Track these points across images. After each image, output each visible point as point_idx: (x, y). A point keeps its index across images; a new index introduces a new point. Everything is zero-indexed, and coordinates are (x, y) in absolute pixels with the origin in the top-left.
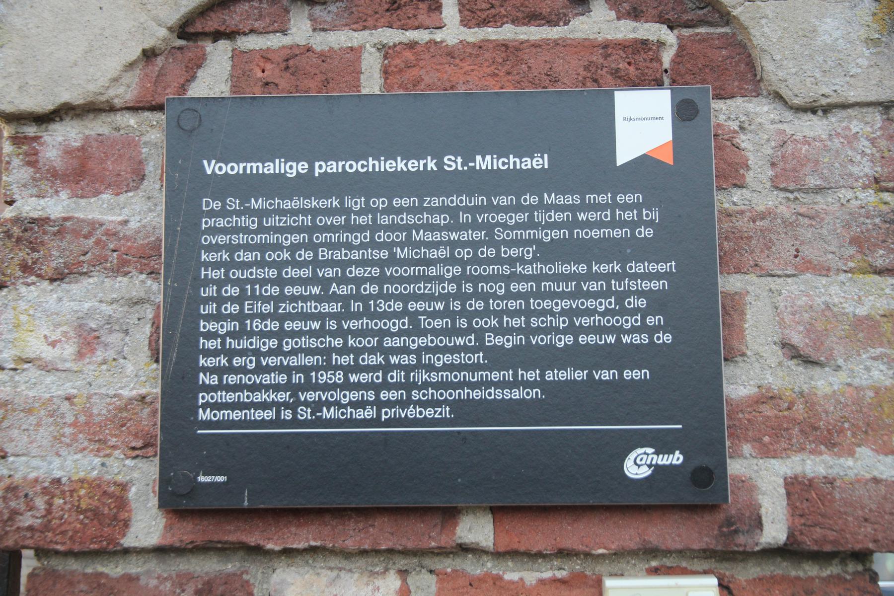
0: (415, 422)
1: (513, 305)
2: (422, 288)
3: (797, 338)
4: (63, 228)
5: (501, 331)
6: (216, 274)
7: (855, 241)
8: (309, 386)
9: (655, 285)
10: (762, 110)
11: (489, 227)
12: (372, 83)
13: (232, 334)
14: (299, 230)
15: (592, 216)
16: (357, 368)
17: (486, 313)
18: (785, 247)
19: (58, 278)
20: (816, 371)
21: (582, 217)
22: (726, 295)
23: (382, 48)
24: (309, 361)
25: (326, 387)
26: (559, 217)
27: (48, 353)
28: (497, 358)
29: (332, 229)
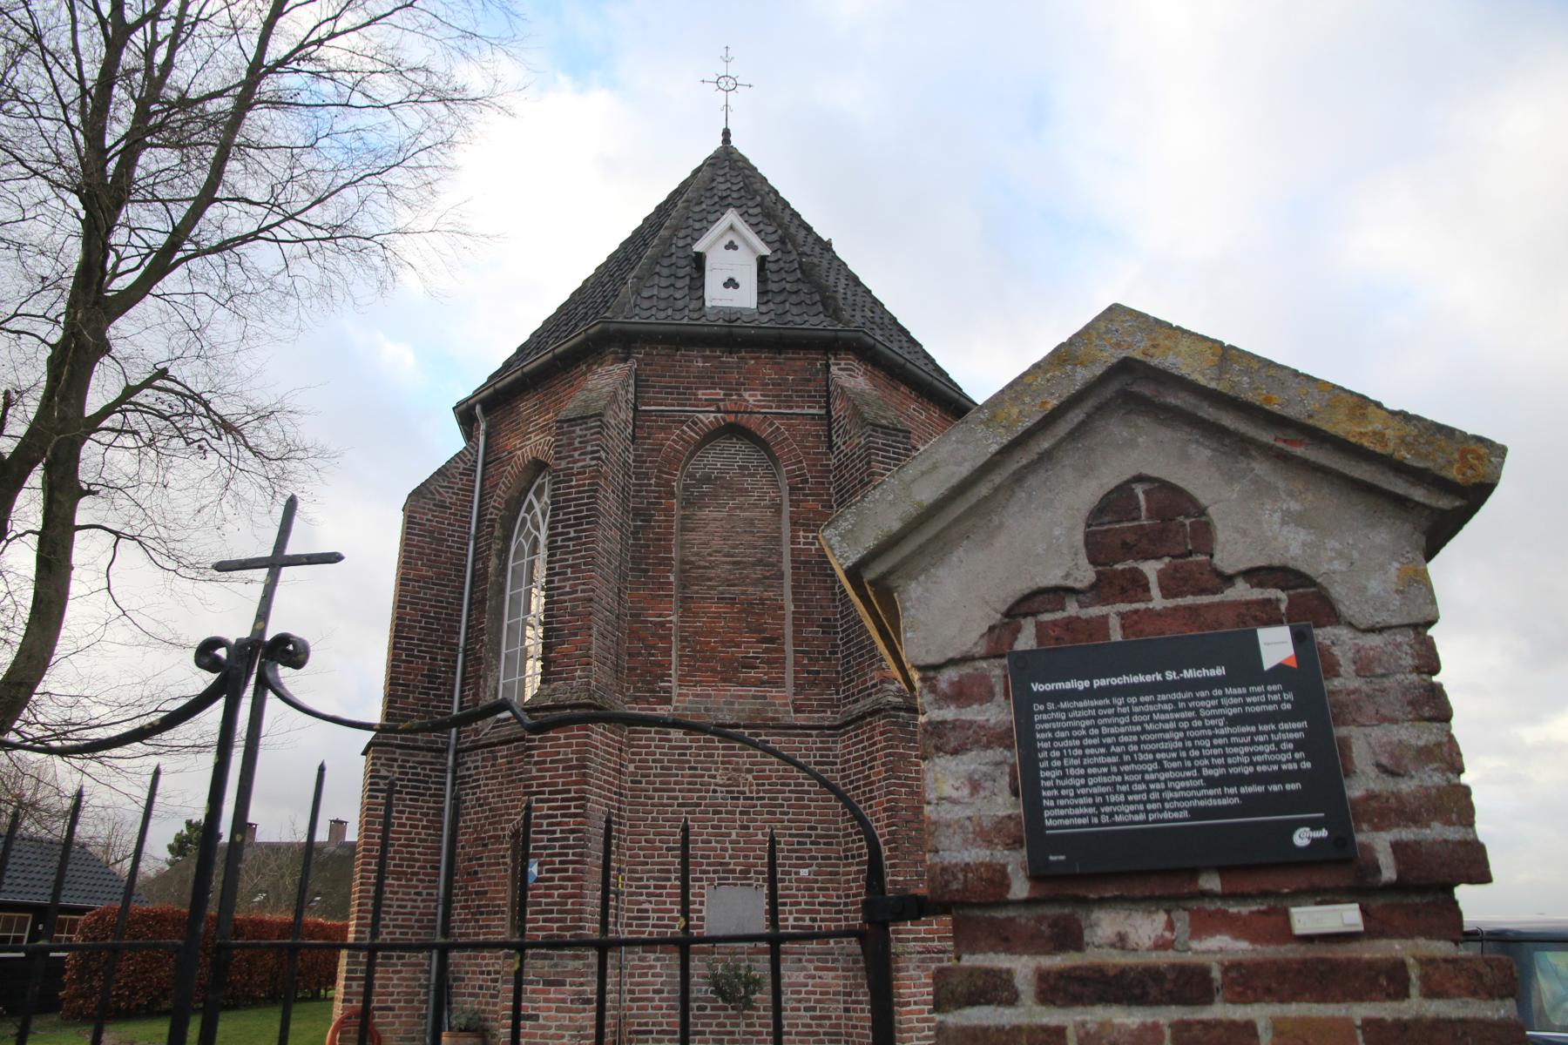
0: (1169, 821)
1: (1216, 752)
2: (1162, 746)
3: (1385, 761)
4: (956, 725)
5: (1211, 766)
6: (1047, 745)
7: (1411, 703)
8: (1105, 804)
9: (1297, 735)
10: (1343, 633)
11: (1196, 710)
12: (1116, 636)
13: (1059, 778)
14: (1089, 718)
15: (1255, 699)
16: (1132, 792)
17: (1201, 757)
18: (1370, 710)
19: (955, 752)
20: (1400, 780)
21: (1249, 700)
22: (1339, 739)
23: (1119, 614)
24: (1104, 790)
25: (1115, 804)
26: (1236, 701)
27: (954, 794)
28: (1211, 782)
29: (1108, 716)
